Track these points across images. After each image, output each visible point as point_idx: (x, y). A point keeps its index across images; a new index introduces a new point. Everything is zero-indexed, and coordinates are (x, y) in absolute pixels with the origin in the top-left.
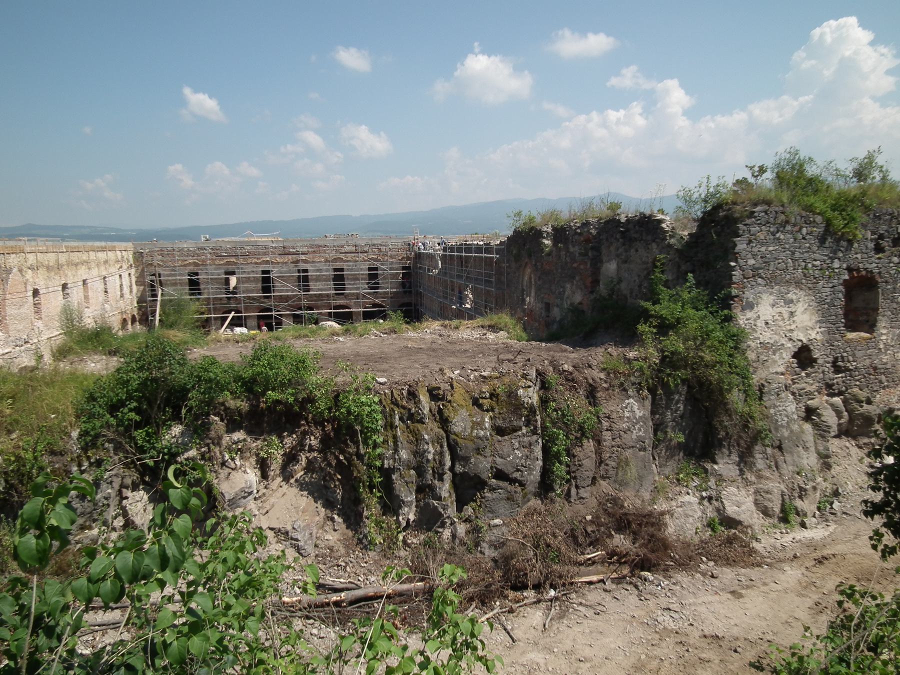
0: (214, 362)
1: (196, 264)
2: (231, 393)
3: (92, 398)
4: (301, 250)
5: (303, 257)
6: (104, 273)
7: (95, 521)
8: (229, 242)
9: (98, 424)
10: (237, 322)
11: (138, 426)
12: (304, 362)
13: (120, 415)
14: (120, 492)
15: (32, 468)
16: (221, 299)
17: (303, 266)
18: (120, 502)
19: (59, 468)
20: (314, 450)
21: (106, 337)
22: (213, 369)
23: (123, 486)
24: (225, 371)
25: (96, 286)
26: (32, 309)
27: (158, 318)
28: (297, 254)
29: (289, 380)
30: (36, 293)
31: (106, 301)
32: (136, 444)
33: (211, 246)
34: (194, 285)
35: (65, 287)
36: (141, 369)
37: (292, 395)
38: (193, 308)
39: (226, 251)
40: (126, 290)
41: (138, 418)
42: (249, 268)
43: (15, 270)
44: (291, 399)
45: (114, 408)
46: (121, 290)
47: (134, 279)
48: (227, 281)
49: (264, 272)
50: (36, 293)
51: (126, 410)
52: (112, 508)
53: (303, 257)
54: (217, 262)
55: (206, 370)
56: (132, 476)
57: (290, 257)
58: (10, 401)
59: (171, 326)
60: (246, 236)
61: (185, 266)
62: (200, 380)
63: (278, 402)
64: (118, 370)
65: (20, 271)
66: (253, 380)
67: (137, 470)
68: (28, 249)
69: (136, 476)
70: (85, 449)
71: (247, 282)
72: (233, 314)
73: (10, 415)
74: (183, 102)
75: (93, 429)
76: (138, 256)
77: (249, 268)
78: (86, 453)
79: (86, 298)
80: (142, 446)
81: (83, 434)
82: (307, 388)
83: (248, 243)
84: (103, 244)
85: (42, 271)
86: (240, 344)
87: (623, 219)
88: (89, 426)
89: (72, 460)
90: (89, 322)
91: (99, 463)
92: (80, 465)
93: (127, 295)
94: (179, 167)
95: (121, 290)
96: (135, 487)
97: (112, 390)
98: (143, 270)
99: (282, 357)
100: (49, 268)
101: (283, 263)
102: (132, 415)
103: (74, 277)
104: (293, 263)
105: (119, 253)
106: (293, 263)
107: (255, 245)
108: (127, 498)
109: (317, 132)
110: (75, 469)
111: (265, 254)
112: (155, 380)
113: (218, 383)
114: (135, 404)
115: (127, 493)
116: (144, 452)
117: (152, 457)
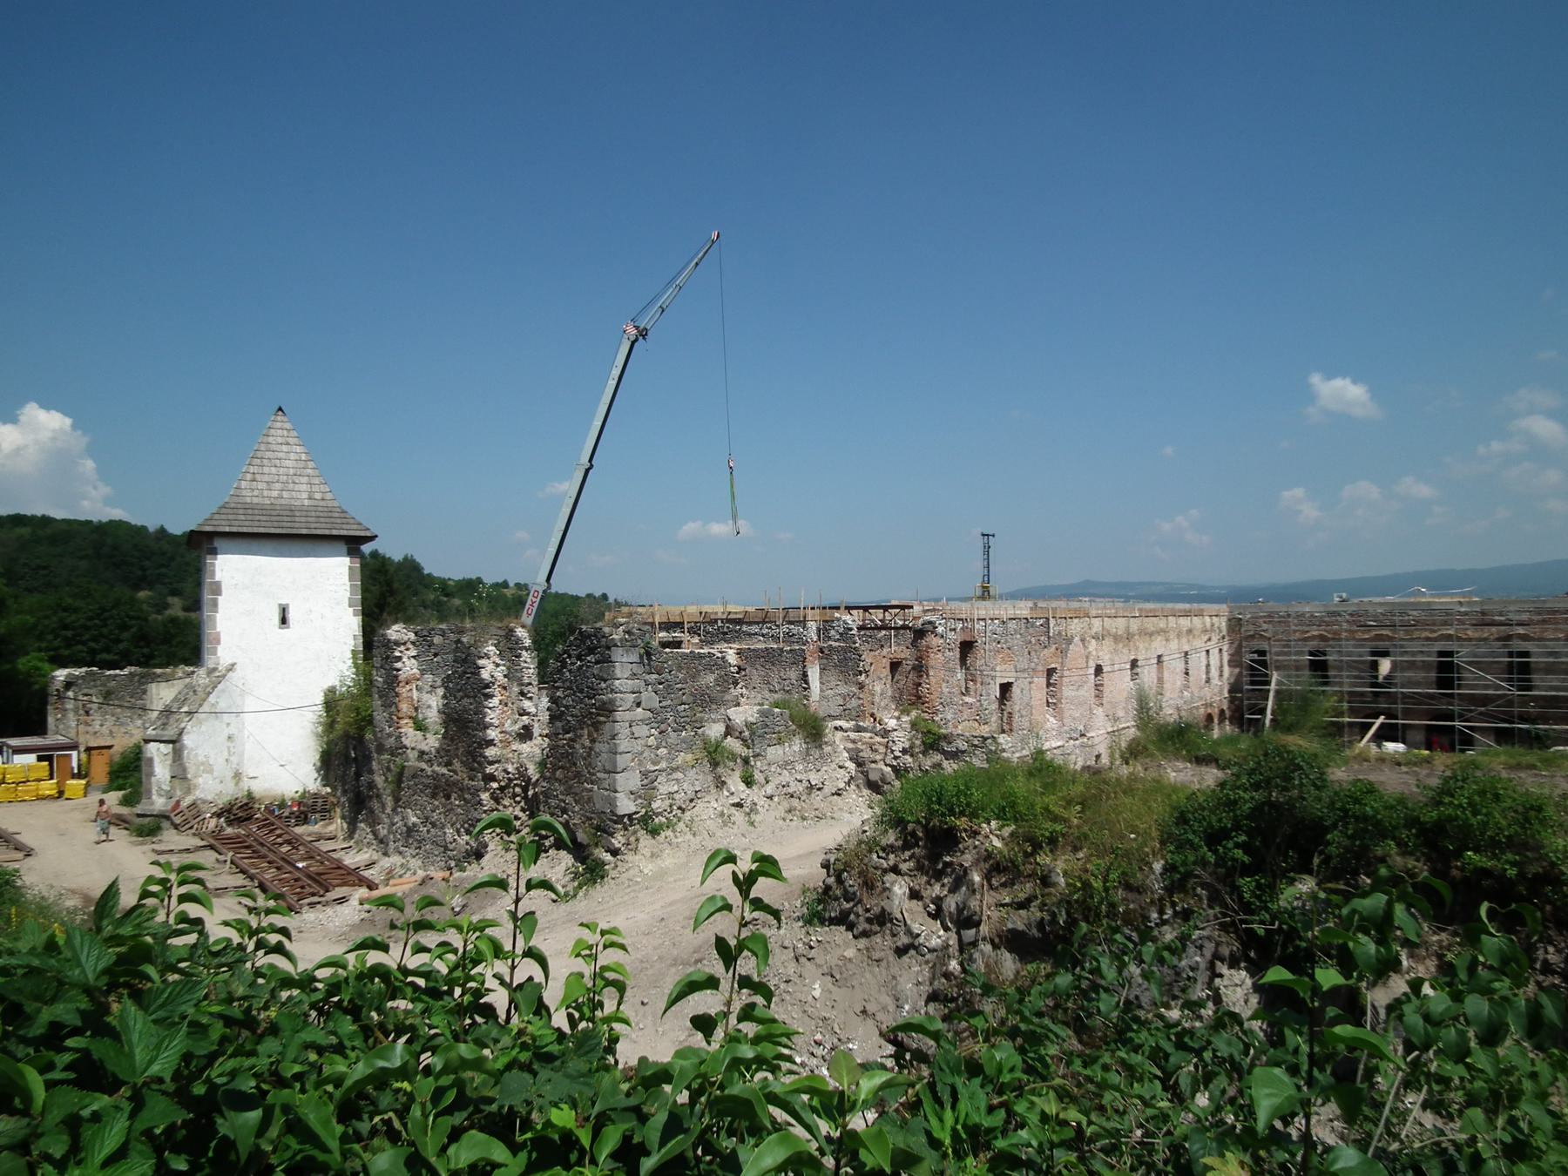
0: (1371, 789)
1: (1322, 638)
2: (1398, 845)
3: (1182, 819)
4: (1515, 617)
5: (1521, 630)
6: (1186, 648)
7: (1175, 998)
8: (1381, 604)
9: (1191, 858)
10: (1386, 734)
11: (1246, 871)
12: (1539, 809)
13: (1221, 850)
14: (1211, 966)
15: (1101, 903)
16: (1362, 694)
17: (1519, 646)
18: (1211, 981)
19: (1135, 910)
20: (1553, 972)
21: (1193, 736)
22: (1368, 799)
23: (1217, 956)
24: (1392, 807)
25: (1175, 665)
26: (1093, 692)
27: (1269, 716)
28: (1508, 624)
29: (1509, 838)
30: (1099, 670)
31: (1187, 687)
32: (1241, 897)
33: (1351, 609)
34: (1319, 667)
35: (1134, 664)
36: (1256, 786)
37: (1513, 864)
38: (1330, 702)
39: (1375, 617)
40: (1214, 673)
41: (1246, 859)
42: (1415, 647)
43: (1077, 639)
44: (1512, 872)
45: (1214, 838)
46: (1208, 672)
47: (1226, 658)
48: (1375, 666)
49: (1441, 654)
50: (1099, 670)
51: (1230, 845)
52: (1199, 986)
53: (1521, 630)
54: (1359, 635)
55: (1357, 801)
56: (1230, 946)
57: (1494, 629)
58: (1078, 808)
59: (1290, 729)
60: (1409, 595)
61: (1305, 639)
62: (1346, 816)
63: (1485, 873)
64: (1222, 785)
65: (1083, 640)
66: (1439, 828)
67: (1239, 938)
68: (1093, 612)
69: (1236, 946)
70: (1170, 890)
71: (1409, 668)
72: (1381, 719)
73: (1079, 827)
74: (1311, 397)
75: (1184, 863)
76: (1235, 624)
77: (1415, 647)
78: (1171, 896)
79: (1160, 680)
80: (1250, 903)
81: (1169, 869)
82: (1544, 857)
83: (1415, 607)
84: (1187, 606)
85: (1108, 642)
86: (1404, 769)
87: (86, 439)
88: (1178, 858)
89: (1152, 902)
90: (1169, 714)
91: (1186, 915)
92: (1161, 912)
93: (1215, 681)
94: (1299, 492)
95: (1208, 672)
96: (1233, 964)
97: (1212, 812)
98: (1240, 646)
99: (1497, 797)
100: (1116, 638)
101: (1480, 639)
102: (1239, 853)
103: (1146, 651)
104: (1498, 639)
105: (1207, 619)
106: (1498, 639)
107: (1428, 608)
108: (1221, 976)
109: (1550, 414)
110: (1155, 915)
111: (1445, 623)
112: (1274, 805)
113: (1378, 824)
114: (1243, 838)
115: (1223, 969)
116: (1252, 913)
117: (1262, 922)
